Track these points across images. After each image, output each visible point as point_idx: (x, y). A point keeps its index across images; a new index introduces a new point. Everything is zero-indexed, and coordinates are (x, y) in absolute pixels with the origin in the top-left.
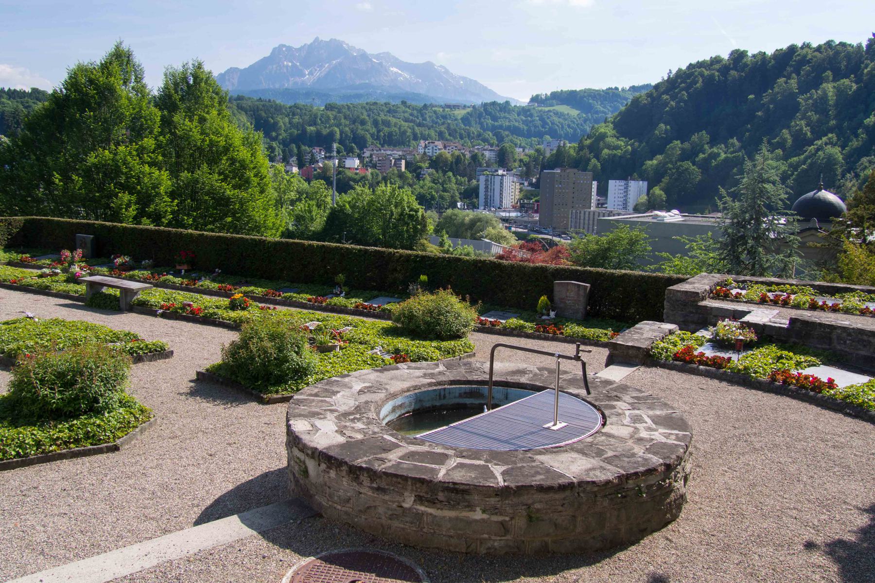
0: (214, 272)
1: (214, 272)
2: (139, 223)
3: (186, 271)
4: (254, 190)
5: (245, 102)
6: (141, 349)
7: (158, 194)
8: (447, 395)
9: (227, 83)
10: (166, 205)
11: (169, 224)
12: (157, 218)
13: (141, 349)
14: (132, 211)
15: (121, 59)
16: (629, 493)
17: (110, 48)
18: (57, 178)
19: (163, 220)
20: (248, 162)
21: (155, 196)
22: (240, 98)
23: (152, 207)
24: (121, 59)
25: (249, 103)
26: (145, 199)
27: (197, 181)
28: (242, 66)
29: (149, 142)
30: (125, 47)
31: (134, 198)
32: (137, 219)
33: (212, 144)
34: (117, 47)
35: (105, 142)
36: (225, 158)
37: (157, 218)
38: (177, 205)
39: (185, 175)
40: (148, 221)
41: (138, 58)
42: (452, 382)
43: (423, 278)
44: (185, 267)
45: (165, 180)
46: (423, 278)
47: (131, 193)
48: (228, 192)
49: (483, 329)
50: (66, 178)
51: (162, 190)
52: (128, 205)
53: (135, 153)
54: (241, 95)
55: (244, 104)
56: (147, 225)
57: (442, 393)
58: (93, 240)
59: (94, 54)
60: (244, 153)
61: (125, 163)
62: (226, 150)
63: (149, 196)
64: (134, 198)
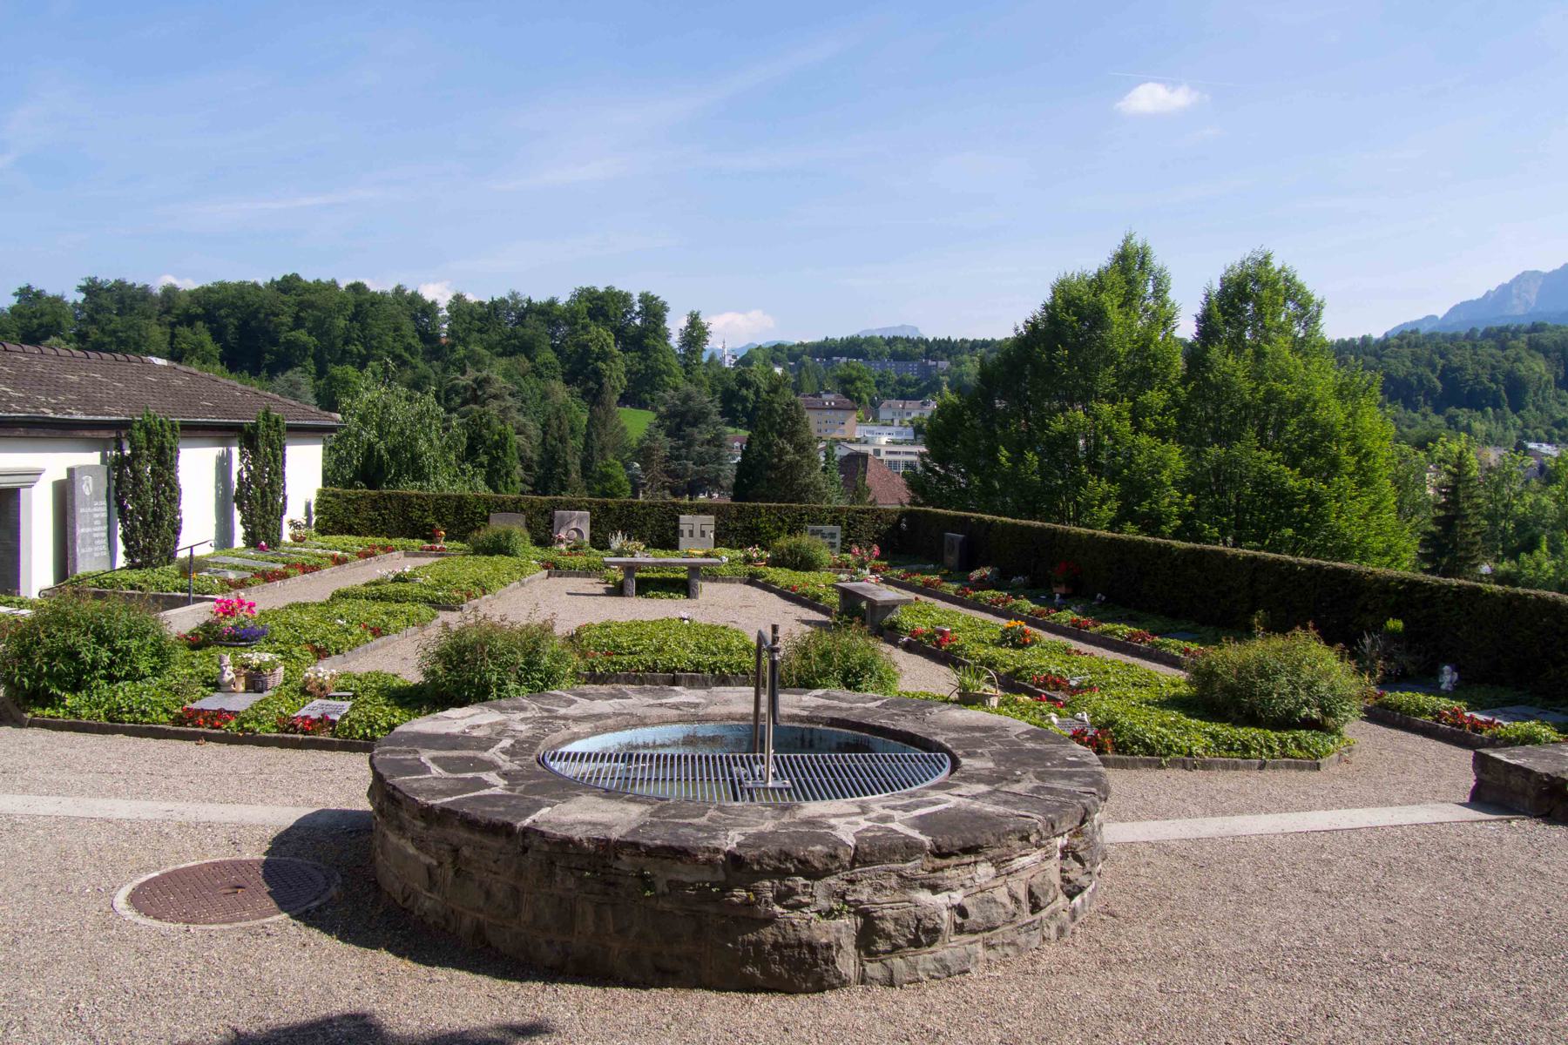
0: (1094, 598)
1: (1094, 598)
2: (1121, 531)
3: (1062, 597)
4: (1344, 482)
5: (1547, 334)
6: (730, 666)
7: (1161, 484)
8: (816, 742)
9: (1515, 302)
10: (1171, 501)
11: (1177, 535)
12: (1152, 523)
13: (730, 666)
14: (1108, 511)
15: (1130, 265)
16: (621, 880)
17: (1113, 246)
18: (1003, 454)
19: (1164, 528)
20: (1339, 428)
21: (1154, 487)
22: (1536, 328)
23: (1145, 506)
24: (1130, 265)
25: (1557, 337)
26: (1135, 491)
27: (1236, 462)
28: (1546, 268)
29: (1155, 398)
30: (1137, 241)
31: (1115, 489)
32: (1114, 524)
33: (1271, 396)
34: (1127, 241)
35: (1087, 396)
36: (1294, 421)
37: (1152, 523)
38: (1192, 504)
39: (1215, 451)
40: (1134, 529)
41: (1158, 260)
42: (834, 722)
43: (1395, 624)
44: (1063, 590)
45: (1175, 458)
46: (1395, 624)
47: (1112, 481)
48: (1291, 482)
49: (1381, 715)
50: (1017, 458)
51: (1165, 476)
52: (1103, 501)
53: (1125, 414)
54: (1538, 320)
55: (1546, 338)
56: (1130, 533)
57: (807, 737)
58: (962, 542)
59: (1089, 258)
60: (1334, 413)
61: (1108, 431)
62: (1299, 407)
63: (1144, 485)
64: (1115, 489)
